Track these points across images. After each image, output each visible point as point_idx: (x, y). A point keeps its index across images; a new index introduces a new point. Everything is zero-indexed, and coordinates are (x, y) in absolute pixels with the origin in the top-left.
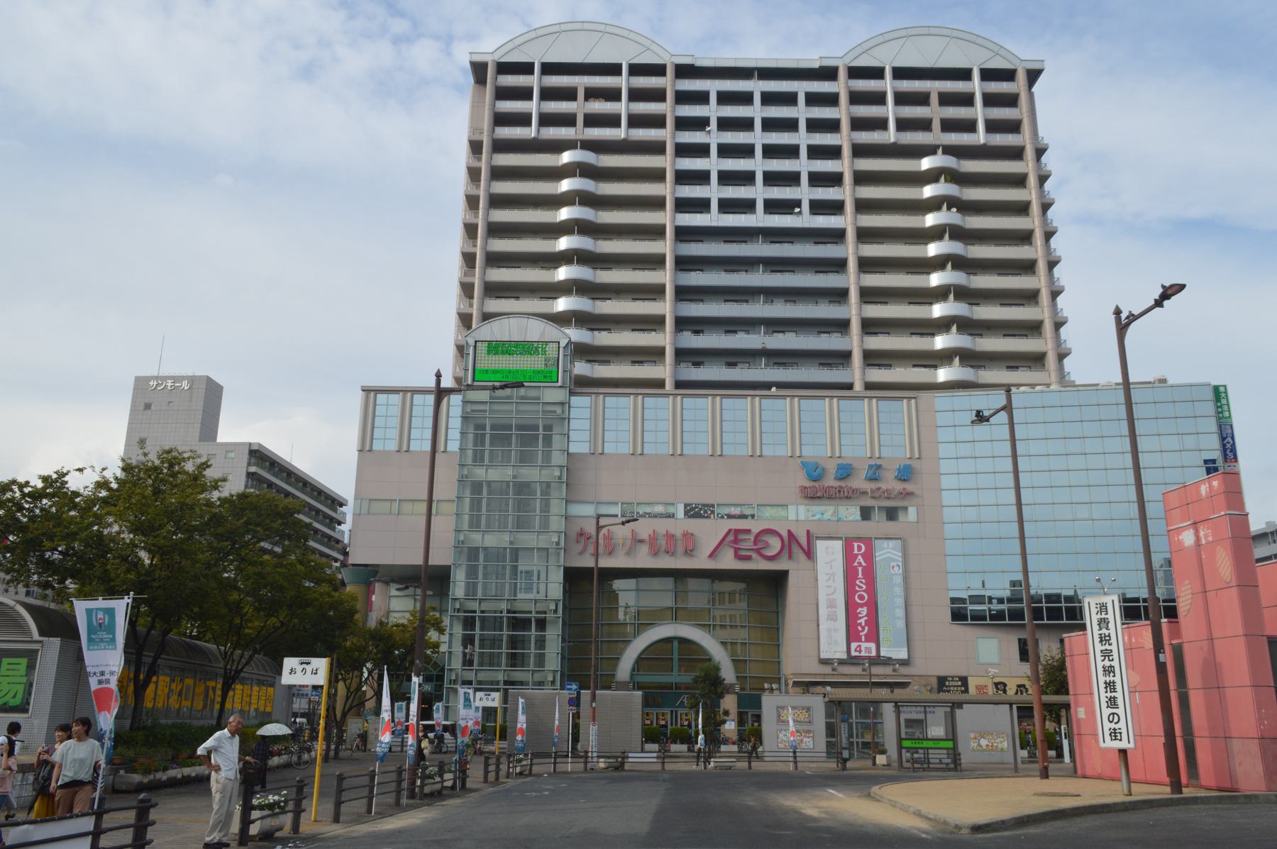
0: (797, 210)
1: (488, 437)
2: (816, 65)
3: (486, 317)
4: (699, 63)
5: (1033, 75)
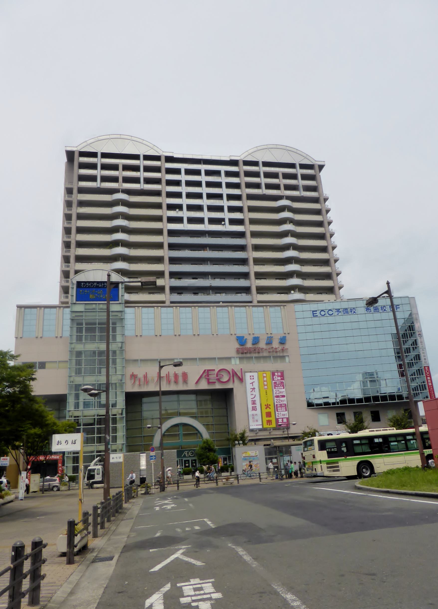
0: (223, 223)
1: (84, 328)
2: (228, 159)
3: (77, 272)
4: (175, 156)
5: (321, 167)
